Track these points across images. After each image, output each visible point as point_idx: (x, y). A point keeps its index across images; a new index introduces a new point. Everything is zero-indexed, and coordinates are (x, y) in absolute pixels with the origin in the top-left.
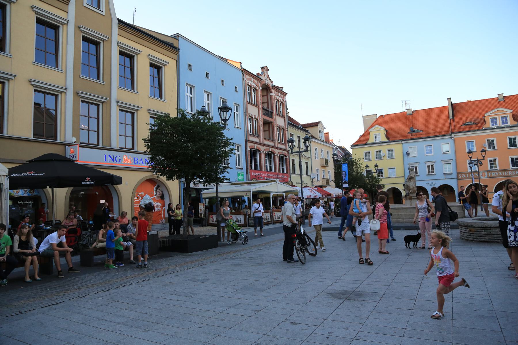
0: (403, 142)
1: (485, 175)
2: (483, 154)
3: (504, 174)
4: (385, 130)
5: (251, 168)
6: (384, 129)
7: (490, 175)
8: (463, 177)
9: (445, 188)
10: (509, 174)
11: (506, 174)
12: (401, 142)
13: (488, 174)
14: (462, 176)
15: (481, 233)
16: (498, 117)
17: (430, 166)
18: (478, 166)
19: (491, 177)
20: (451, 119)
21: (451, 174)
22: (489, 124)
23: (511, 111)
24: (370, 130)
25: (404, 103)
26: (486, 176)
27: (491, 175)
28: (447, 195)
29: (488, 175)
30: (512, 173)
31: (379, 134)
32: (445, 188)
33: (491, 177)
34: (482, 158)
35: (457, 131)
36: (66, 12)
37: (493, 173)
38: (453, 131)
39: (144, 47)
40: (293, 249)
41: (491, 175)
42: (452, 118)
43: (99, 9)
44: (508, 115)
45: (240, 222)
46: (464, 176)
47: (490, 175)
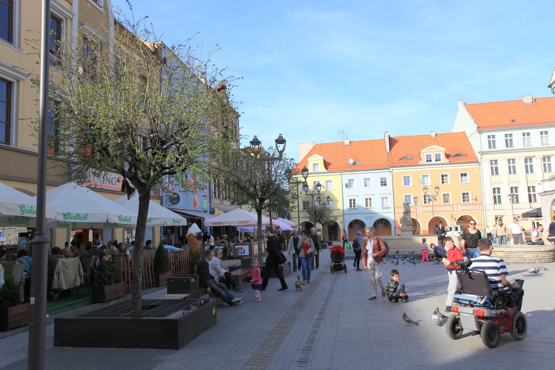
0: (342, 173)
1: (420, 210)
2: (437, 190)
4: (324, 159)
5: (215, 196)
6: (323, 158)
7: (424, 210)
8: (399, 211)
9: (380, 223)
10: (441, 210)
11: (438, 210)
12: (340, 173)
13: (422, 208)
14: (398, 210)
15: (508, 256)
17: (368, 199)
18: (432, 202)
19: (426, 212)
20: (388, 153)
21: (389, 208)
22: (424, 161)
23: (444, 149)
24: (309, 159)
25: (341, 132)
26: (421, 211)
27: (425, 210)
28: (382, 230)
29: (423, 210)
30: (444, 209)
31: (318, 164)
32: (380, 223)
33: (426, 212)
34: (436, 194)
35: (394, 165)
36: (68, 3)
37: (427, 208)
38: (391, 165)
39: (22, 24)
40: (186, 294)
41: (425, 210)
42: (389, 151)
43: (97, 1)
45: (244, 253)
47: (424, 210)
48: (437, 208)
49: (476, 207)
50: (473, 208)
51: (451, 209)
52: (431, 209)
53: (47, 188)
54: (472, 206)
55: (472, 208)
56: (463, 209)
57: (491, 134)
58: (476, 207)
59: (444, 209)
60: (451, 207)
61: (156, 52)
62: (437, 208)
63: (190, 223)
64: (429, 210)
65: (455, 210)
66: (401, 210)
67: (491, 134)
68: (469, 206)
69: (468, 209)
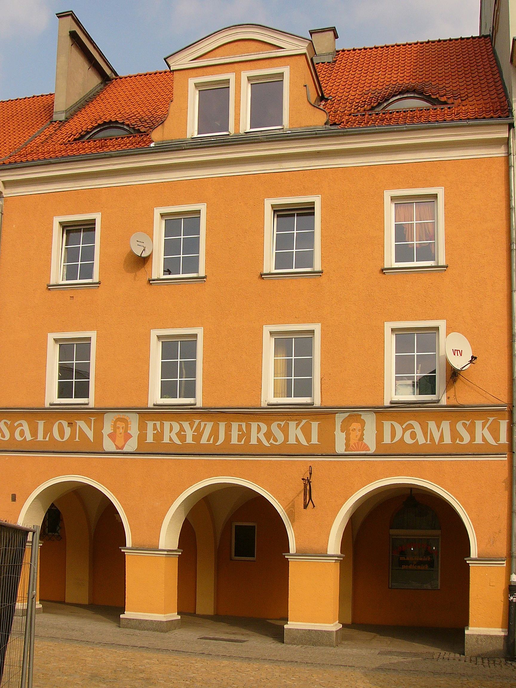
1: (128, 437)
3: (215, 433)
7: (150, 439)
10: (254, 441)
11: (234, 440)
13: (142, 428)
16: (231, 77)
27: (159, 436)
29: (142, 437)
30: (269, 435)
37: (167, 424)
41: (159, 436)
44: (286, 70)
46: (22, 433)
47: (150, 439)
48: (228, 429)
49: (472, 432)
50: (455, 434)
51: (315, 440)
52: (11, 667)
53: (159, 548)
54: (446, 425)
55: (447, 440)
56: (387, 439)
57: (240, 423)
58: (285, 431)
59: (269, 435)
60: (315, 425)
61: (513, 379)
62: (228, 429)
63: (155, 432)
64: (181, 435)
65: (340, 448)
66: (26, 427)
67: (240, 423)
68: (432, 425)
69: (421, 440)
